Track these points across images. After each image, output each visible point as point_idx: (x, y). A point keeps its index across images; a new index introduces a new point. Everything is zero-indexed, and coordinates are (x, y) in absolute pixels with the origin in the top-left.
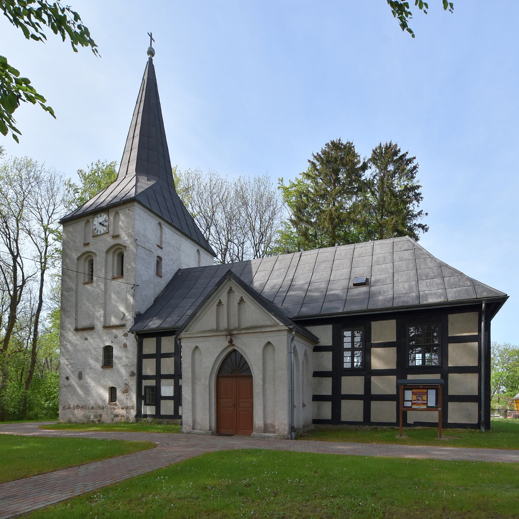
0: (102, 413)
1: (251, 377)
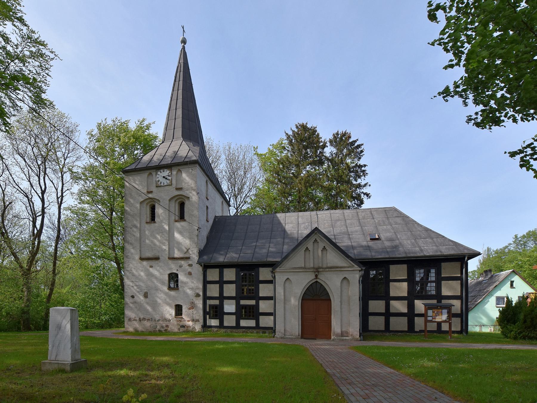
0: (168, 325)
1: (330, 300)
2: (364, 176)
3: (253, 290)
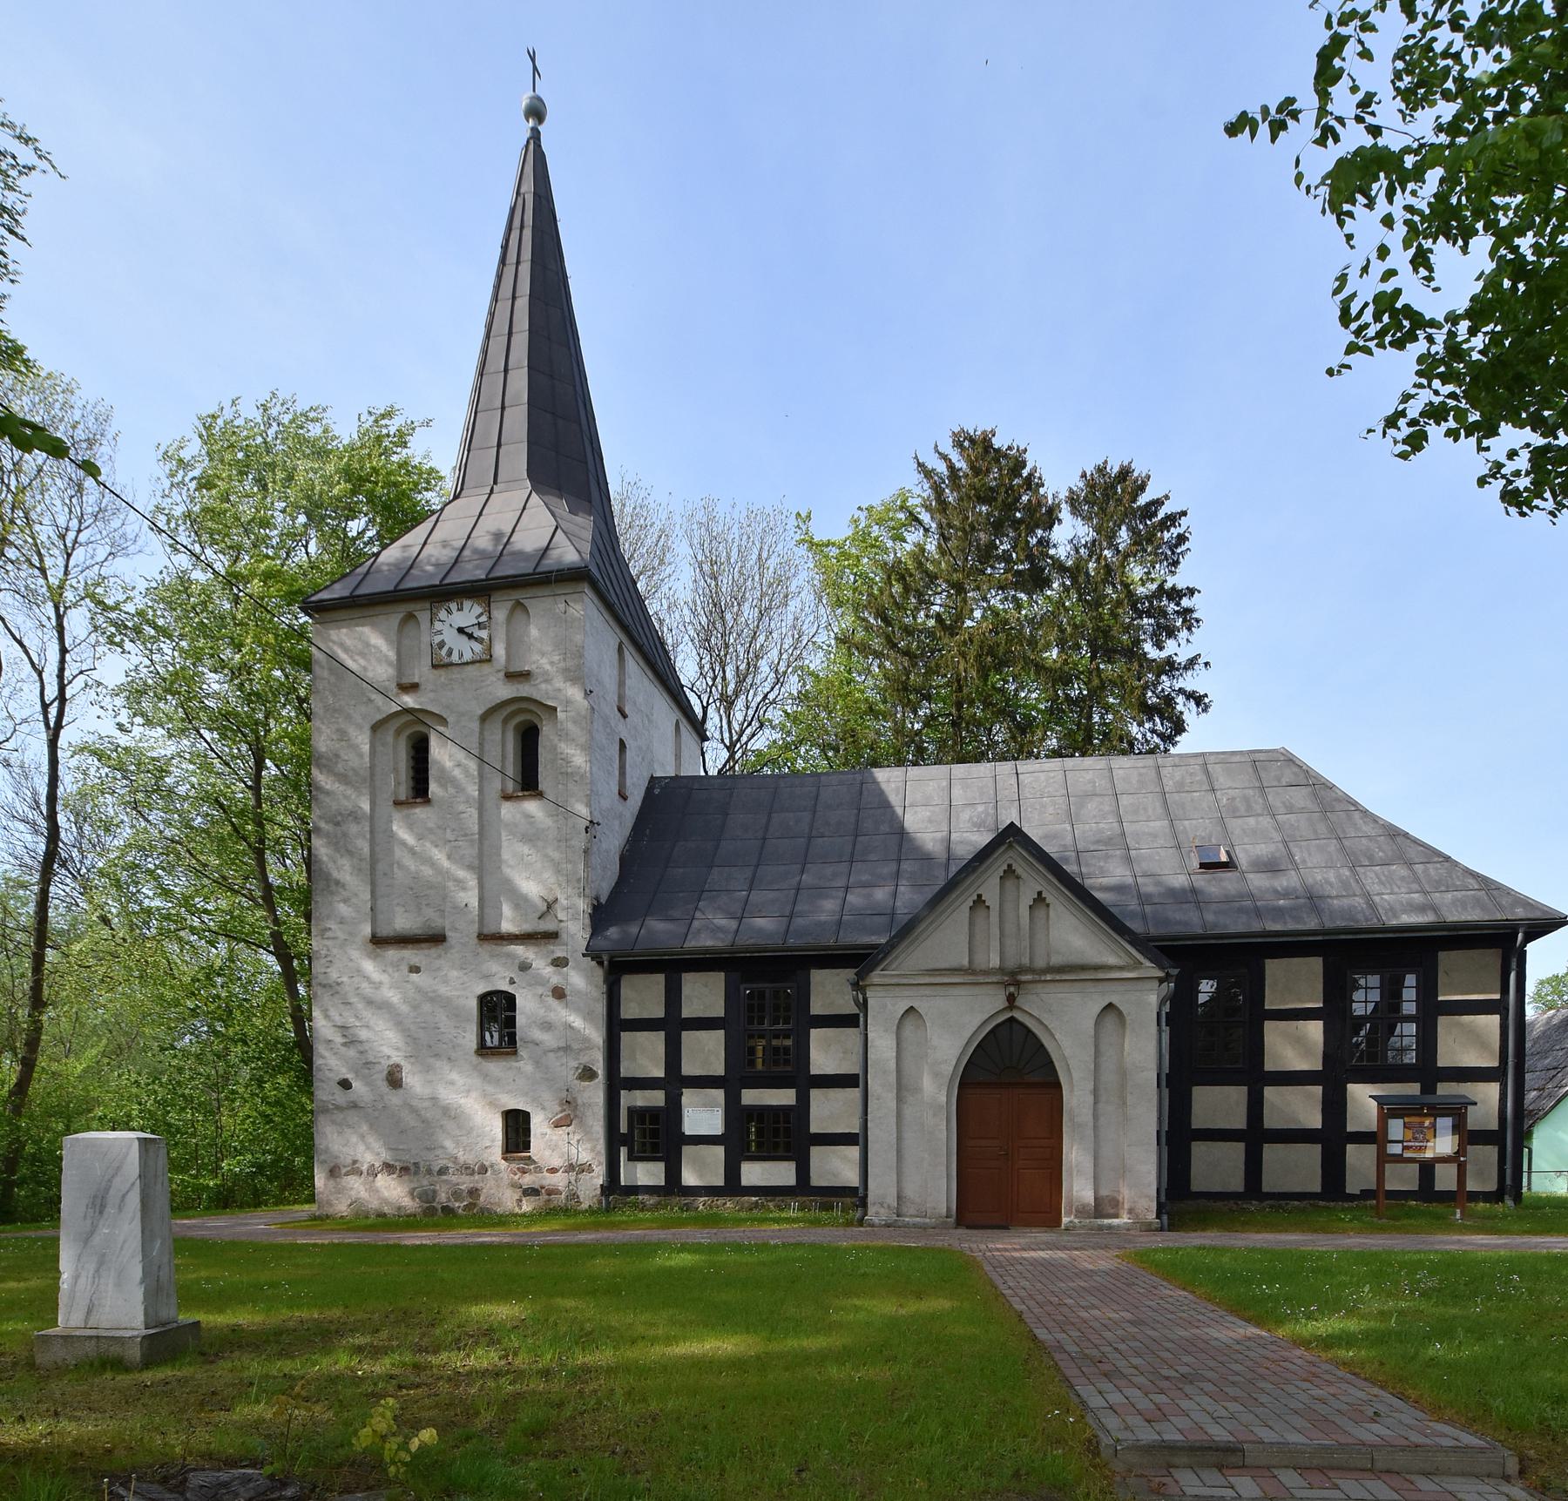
0: (479, 1186)
1: (1058, 1086)
2: (1189, 629)
3: (786, 1050)
